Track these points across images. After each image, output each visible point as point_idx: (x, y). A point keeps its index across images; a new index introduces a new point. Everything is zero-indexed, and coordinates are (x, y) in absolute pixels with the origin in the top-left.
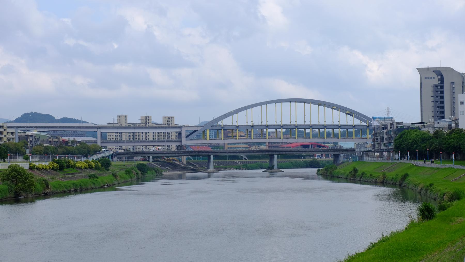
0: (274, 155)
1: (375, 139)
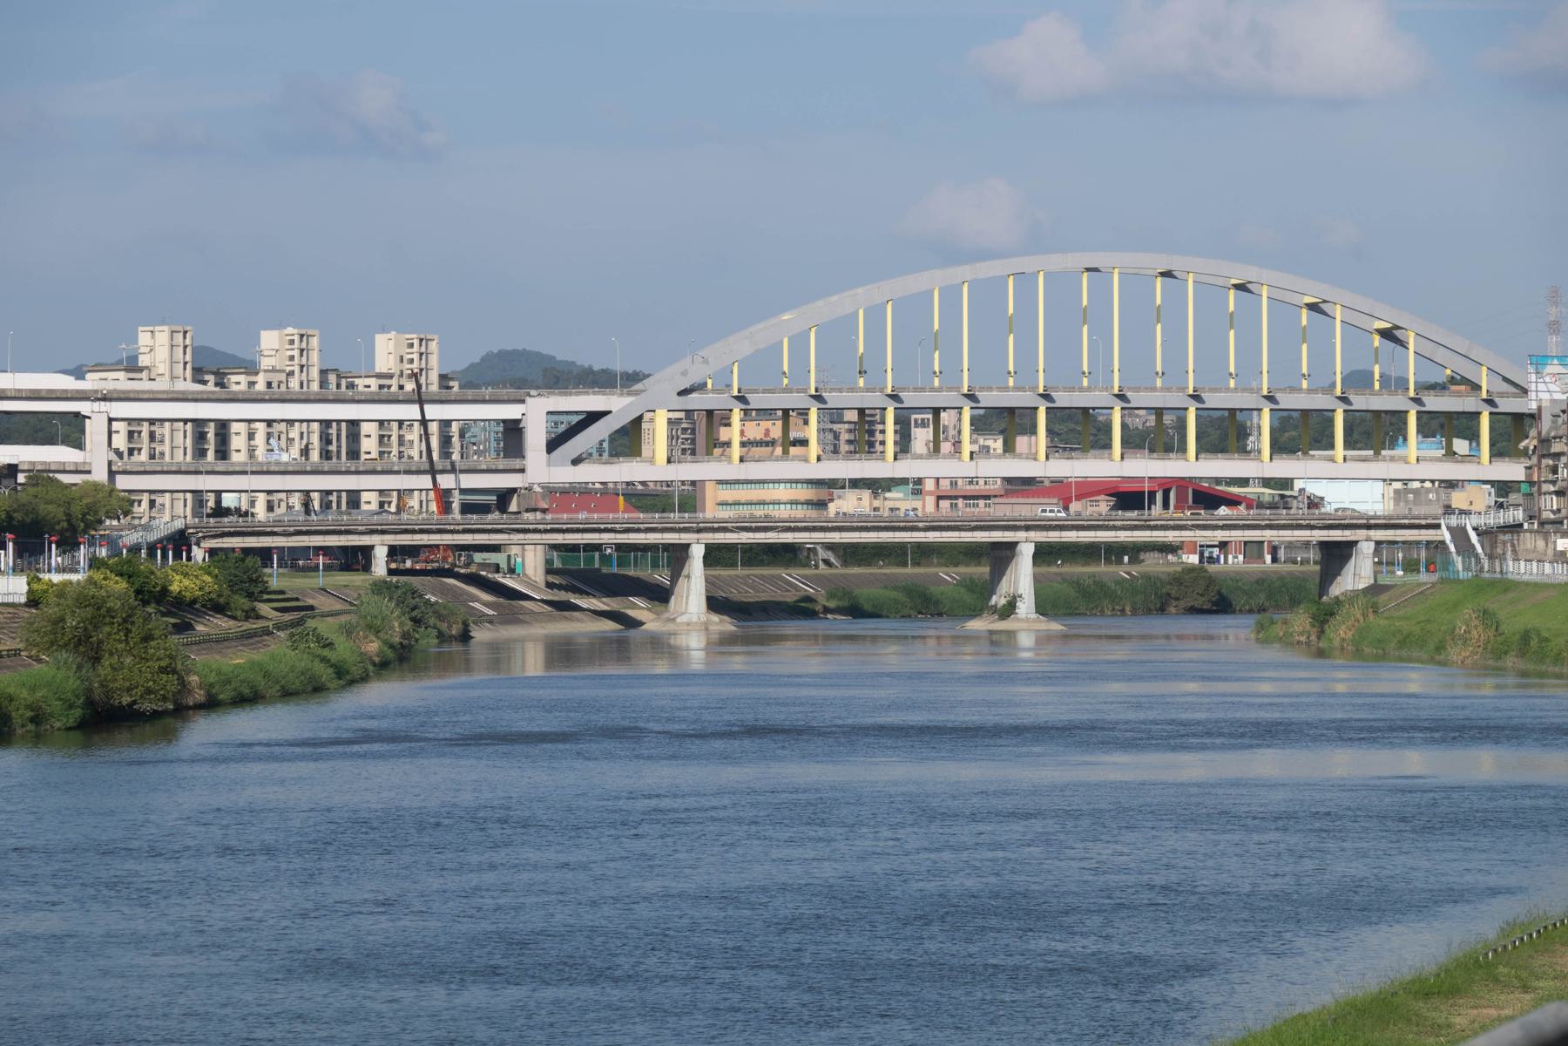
0: (1016, 543)
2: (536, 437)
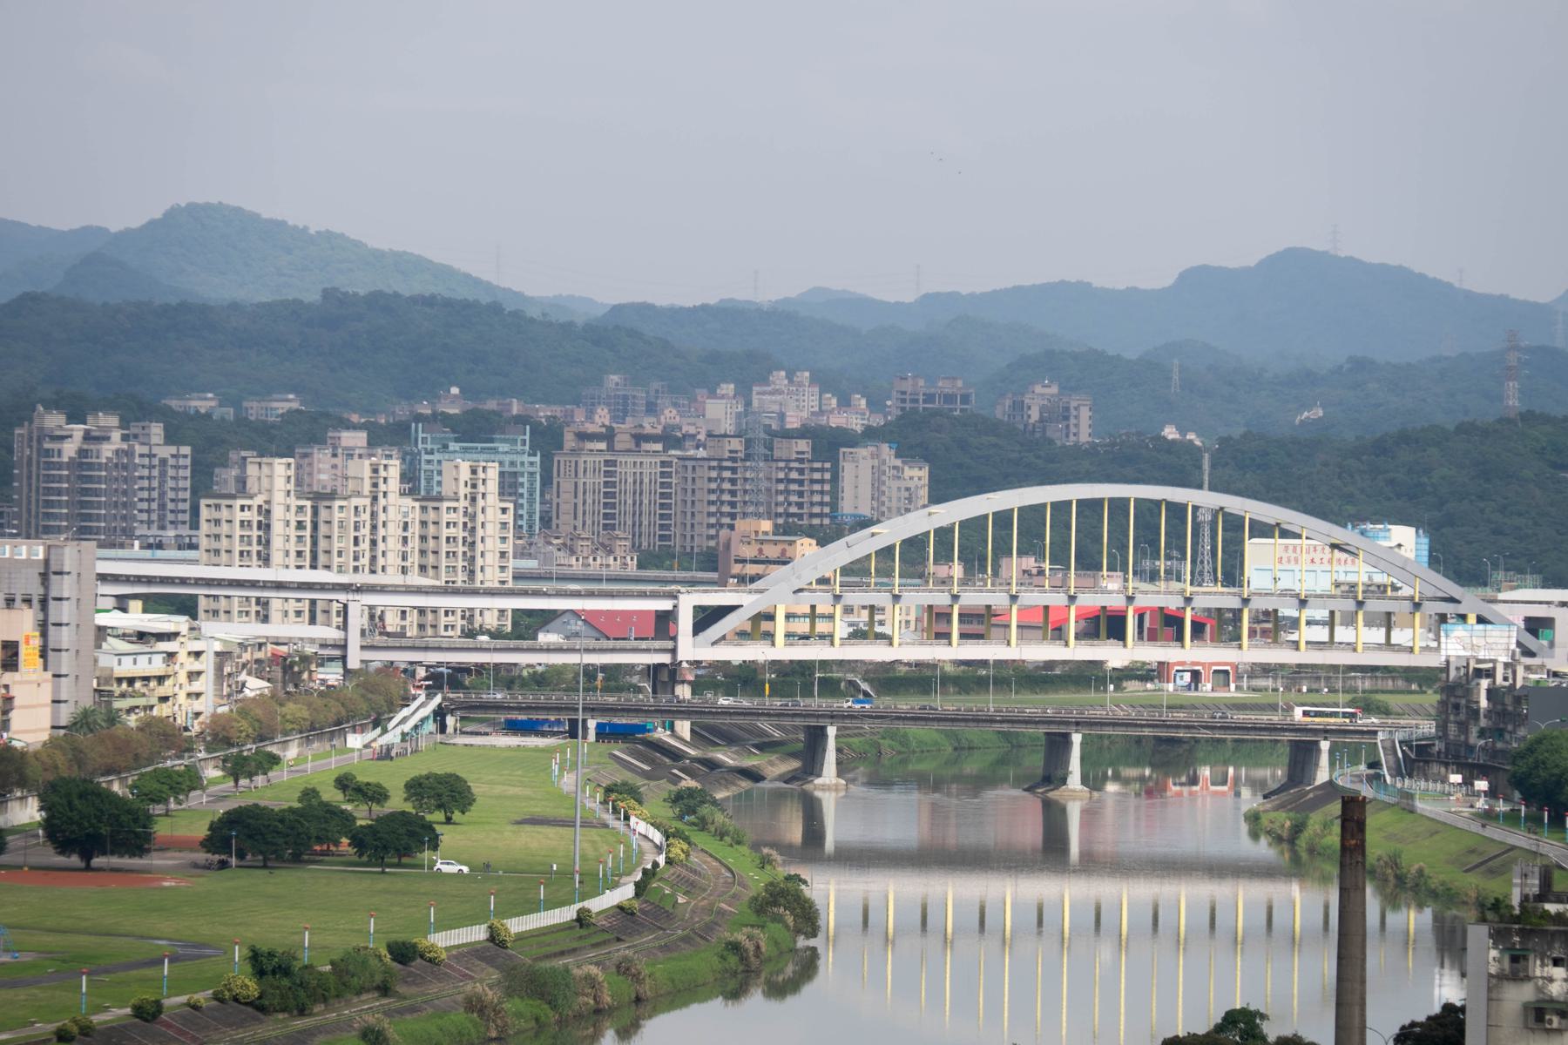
1: (1450, 706)
2: (685, 621)
